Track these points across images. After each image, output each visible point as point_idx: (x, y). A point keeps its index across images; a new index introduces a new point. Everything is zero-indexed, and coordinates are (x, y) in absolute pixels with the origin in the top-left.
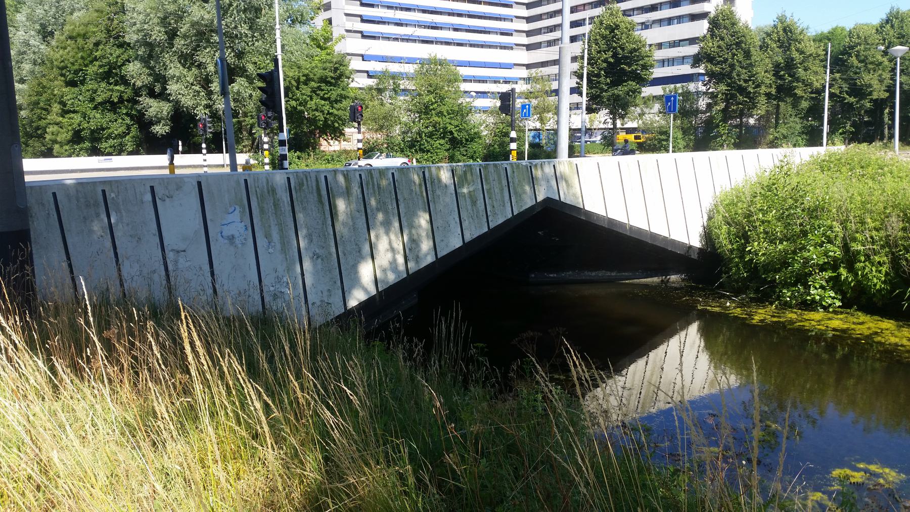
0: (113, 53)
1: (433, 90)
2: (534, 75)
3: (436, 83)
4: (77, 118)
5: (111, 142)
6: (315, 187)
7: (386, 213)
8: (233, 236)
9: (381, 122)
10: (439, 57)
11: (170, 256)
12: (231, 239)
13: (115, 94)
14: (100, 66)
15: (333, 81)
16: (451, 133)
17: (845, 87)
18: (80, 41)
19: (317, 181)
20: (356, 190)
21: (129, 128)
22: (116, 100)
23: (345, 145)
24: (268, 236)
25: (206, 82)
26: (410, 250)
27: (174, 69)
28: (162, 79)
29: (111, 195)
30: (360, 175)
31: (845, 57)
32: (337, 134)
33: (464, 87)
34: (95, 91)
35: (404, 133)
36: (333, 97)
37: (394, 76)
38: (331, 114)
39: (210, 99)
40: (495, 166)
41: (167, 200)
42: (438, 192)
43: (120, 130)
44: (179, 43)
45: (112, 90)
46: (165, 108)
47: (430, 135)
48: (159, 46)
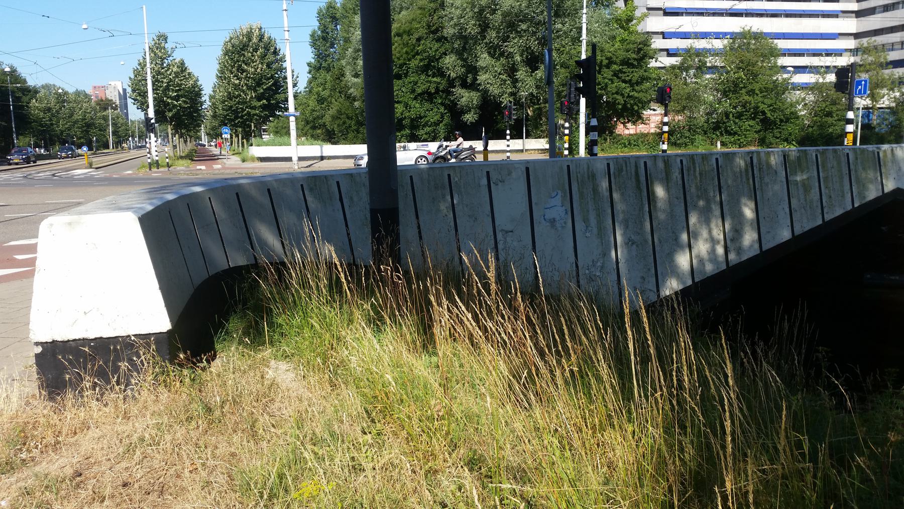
0: (431, 46)
1: (746, 66)
2: (866, 45)
3: (751, 58)
5: (428, 129)
6: (633, 173)
7: (708, 201)
8: (554, 219)
9: (684, 103)
10: (754, 29)
11: (500, 236)
12: (553, 222)
13: (433, 85)
14: (421, 60)
15: (635, 63)
16: (764, 113)
18: (405, 37)
19: (636, 167)
20: (676, 174)
21: (442, 117)
22: (433, 91)
23: (641, 128)
24: (586, 220)
25: (512, 71)
26: (732, 240)
27: (484, 60)
28: (474, 70)
29: (455, 179)
30: (681, 161)
32: (636, 117)
33: (783, 61)
34: (416, 83)
35: (707, 114)
36: (634, 80)
37: (699, 53)
38: (631, 97)
39: (515, 87)
40: (835, 151)
41: (500, 184)
42: (767, 179)
43: (435, 118)
44: (492, 34)
45: (430, 82)
47: (739, 116)
48: (472, 39)
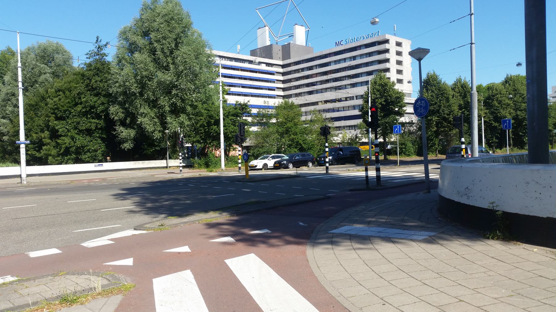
4: (67, 140)
17: (491, 117)
22: (94, 128)
31: (490, 101)
46: (132, 133)
